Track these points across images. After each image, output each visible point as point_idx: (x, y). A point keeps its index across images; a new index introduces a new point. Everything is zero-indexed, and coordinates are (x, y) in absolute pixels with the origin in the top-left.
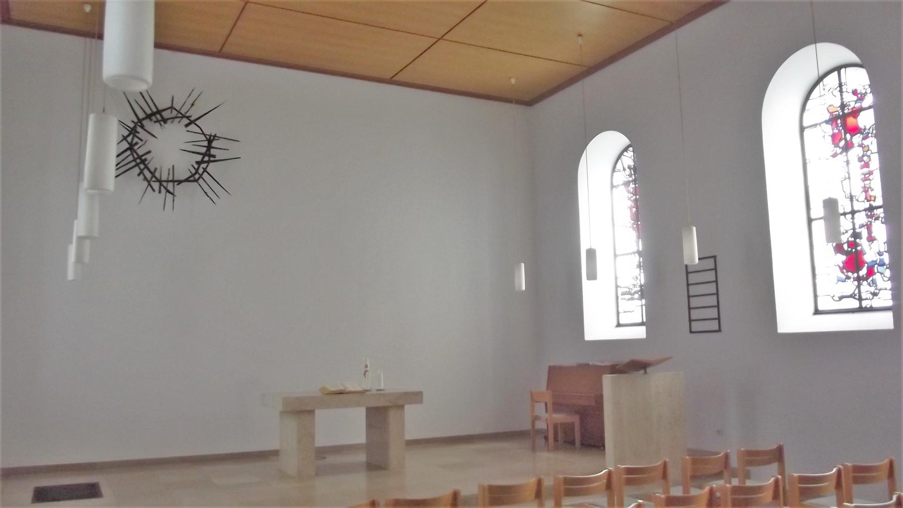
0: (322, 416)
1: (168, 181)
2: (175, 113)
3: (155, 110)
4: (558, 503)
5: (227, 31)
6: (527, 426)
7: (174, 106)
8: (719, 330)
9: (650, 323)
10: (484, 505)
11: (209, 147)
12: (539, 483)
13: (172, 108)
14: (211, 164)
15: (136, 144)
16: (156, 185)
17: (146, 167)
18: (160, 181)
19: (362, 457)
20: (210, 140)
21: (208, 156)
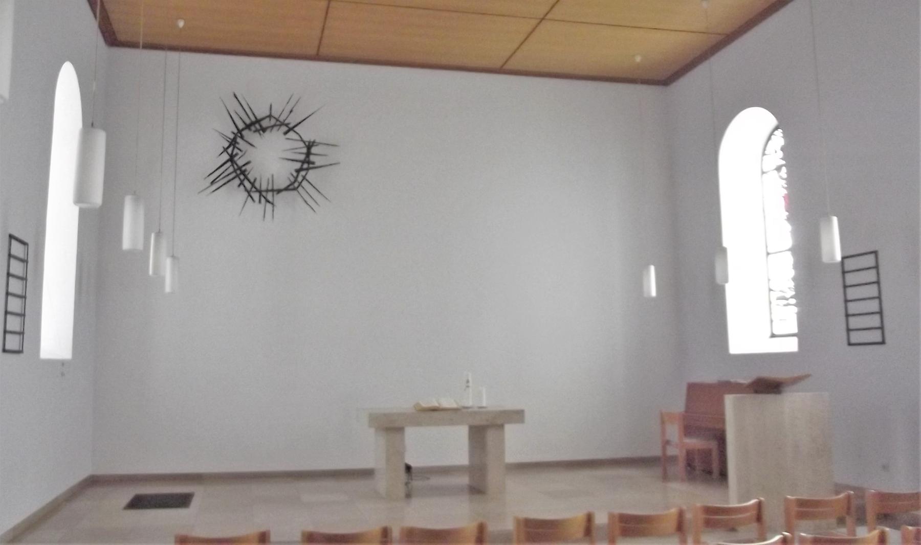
0: (411, 434)
1: (267, 191)
2: (273, 122)
3: (253, 119)
4: (697, 541)
5: (516, 46)
6: (657, 452)
7: (274, 114)
8: (883, 342)
9: (802, 335)
10: (519, 541)
11: (308, 154)
12: (589, 518)
13: (270, 116)
14: (310, 171)
15: (237, 154)
16: (256, 196)
17: (246, 177)
18: (260, 192)
19: (464, 480)
20: (310, 146)
21: (307, 163)
